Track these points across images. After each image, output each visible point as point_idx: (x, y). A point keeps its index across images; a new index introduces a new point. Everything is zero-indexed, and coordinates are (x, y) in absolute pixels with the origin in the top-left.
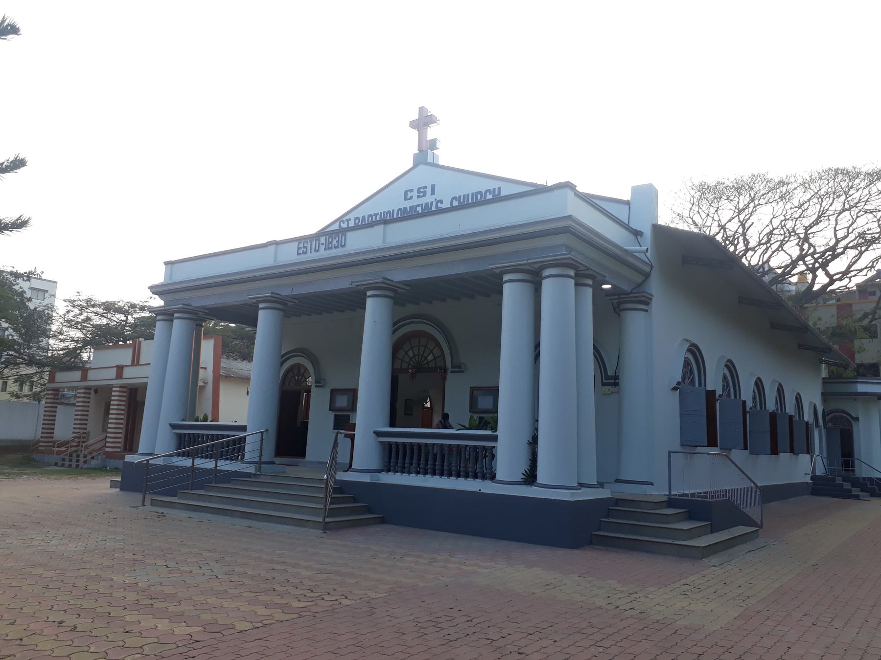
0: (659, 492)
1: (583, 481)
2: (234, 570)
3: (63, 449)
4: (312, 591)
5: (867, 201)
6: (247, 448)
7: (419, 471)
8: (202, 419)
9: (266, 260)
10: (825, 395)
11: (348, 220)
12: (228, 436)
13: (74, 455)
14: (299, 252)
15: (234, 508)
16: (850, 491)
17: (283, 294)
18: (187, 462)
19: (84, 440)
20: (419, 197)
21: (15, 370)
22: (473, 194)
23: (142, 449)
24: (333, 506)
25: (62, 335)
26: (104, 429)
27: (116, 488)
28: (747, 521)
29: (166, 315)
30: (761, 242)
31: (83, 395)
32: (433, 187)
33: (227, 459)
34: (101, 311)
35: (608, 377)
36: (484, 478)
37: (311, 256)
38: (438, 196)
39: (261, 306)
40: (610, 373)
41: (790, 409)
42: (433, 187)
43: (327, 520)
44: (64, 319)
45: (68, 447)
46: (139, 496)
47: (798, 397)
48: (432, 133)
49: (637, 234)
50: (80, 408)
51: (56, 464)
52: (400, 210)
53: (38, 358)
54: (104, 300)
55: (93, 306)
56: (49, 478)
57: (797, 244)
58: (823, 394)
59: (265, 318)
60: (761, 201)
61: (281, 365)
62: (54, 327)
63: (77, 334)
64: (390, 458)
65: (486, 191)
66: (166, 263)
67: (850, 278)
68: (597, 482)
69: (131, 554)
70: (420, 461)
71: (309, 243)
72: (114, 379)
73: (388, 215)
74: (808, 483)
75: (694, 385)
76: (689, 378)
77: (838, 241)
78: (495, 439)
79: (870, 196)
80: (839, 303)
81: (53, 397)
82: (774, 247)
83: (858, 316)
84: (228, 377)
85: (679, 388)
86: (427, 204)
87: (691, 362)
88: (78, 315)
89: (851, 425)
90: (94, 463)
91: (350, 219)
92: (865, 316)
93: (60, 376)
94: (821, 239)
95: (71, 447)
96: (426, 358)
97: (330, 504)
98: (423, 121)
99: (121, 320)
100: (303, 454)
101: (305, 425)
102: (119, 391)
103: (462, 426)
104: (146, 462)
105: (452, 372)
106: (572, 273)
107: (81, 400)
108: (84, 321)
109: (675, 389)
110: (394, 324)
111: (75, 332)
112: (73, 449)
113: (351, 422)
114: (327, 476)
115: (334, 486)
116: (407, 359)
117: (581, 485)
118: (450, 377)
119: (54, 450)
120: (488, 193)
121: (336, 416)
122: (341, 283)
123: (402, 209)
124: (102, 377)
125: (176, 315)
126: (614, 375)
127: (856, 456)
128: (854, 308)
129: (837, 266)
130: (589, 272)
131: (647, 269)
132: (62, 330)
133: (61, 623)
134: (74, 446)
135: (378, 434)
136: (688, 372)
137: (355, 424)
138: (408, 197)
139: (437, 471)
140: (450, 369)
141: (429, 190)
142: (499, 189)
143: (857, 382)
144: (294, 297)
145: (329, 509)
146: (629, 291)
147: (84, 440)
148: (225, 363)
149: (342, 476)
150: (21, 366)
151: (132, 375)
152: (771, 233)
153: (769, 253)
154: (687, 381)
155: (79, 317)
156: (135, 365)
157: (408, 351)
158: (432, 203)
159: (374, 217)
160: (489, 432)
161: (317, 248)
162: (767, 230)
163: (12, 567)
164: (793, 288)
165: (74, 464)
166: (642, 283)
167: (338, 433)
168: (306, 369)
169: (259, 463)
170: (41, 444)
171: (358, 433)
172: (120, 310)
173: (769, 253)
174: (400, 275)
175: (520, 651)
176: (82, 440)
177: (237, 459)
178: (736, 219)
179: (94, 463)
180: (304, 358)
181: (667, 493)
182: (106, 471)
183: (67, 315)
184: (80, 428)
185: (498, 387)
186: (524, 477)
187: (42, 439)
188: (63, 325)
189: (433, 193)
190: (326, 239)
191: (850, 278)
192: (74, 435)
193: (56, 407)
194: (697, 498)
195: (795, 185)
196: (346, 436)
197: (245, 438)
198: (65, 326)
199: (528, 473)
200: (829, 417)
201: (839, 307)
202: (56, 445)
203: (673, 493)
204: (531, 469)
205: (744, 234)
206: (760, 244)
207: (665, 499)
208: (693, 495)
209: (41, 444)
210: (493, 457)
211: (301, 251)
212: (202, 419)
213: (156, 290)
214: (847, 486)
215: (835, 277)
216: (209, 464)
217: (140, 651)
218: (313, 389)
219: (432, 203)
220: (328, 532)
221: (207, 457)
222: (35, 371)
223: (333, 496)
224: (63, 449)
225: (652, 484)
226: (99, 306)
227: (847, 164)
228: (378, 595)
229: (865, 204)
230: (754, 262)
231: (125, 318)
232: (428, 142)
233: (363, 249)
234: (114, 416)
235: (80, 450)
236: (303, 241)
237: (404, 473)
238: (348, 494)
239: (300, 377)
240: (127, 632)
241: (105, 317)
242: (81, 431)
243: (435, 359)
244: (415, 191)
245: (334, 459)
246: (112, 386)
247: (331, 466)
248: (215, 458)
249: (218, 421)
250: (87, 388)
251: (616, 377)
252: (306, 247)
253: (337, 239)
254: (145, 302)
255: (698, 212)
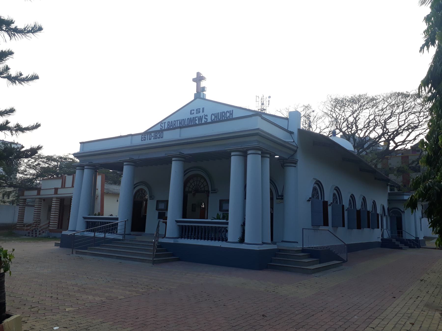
0: (299, 246)
1: (265, 241)
2: (115, 279)
3: (28, 228)
4: (148, 286)
5: (414, 107)
6: (119, 228)
7: (195, 238)
8: (97, 214)
9: (127, 143)
10: (389, 201)
11: (165, 123)
12: (110, 223)
13: (34, 231)
14: (142, 140)
15: (113, 255)
16: (398, 245)
17: (134, 158)
18: (92, 234)
19: (39, 223)
20: (197, 113)
21: (3, 189)
22: (221, 113)
23: (70, 228)
24: (157, 253)
25: (26, 172)
26: (48, 218)
27: (58, 246)
28: (338, 258)
29: (82, 167)
30: (365, 127)
31: (38, 202)
32: (203, 109)
33: (109, 233)
34: (45, 160)
35: (279, 196)
36: (223, 240)
37: (147, 142)
38: (205, 113)
39: (125, 164)
40: (280, 194)
41: (369, 208)
42: (203, 109)
43: (154, 259)
44: (27, 164)
45: (31, 227)
46: (71, 250)
47: (364, 198)
48: (203, 84)
49: (291, 133)
50: (37, 208)
51: (25, 235)
52: (188, 119)
53: (14, 183)
54: (46, 155)
55: (41, 158)
56: (25, 242)
57: (381, 128)
58: (388, 200)
59: (126, 169)
60: (364, 108)
61: (134, 189)
62: (22, 168)
63: (32, 171)
64: (182, 232)
65: (227, 112)
66: (81, 143)
67: (406, 144)
68: (262, 242)
69: (72, 273)
70: (206, 234)
71: (147, 136)
72: (53, 195)
73: (183, 121)
74: (379, 242)
75: (318, 199)
76: (316, 195)
77: (400, 127)
78: (227, 223)
79: (415, 105)
80: (402, 155)
81: (23, 203)
82: (371, 129)
83: (410, 162)
84: (108, 193)
85: (310, 200)
86: (200, 116)
87: (317, 188)
88: (34, 162)
89: (401, 215)
90: (44, 234)
91: (165, 122)
92: (413, 162)
93: (27, 193)
94: (392, 126)
95: (33, 227)
96: (200, 186)
97: (156, 253)
98: (199, 79)
99: (55, 165)
100: (144, 230)
101: (145, 217)
102: (56, 200)
103: (214, 218)
104: (73, 234)
105: (211, 193)
106: (260, 152)
107: (37, 204)
108: (37, 165)
109: (309, 201)
110: (185, 172)
111: (32, 171)
112: (33, 228)
113: (166, 216)
114: (154, 240)
115: (158, 245)
116: (191, 187)
117: (263, 243)
118: (210, 195)
119: (24, 229)
120: (228, 113)
121: (159, 213)
122: (161, 154)
123: (189, 118)
124: (47, 193)
125: (85, 167)
126: (281, 195)
127: (403, 229)
128: (410, 158)
129: (398, 139)
130: (268, 152)
131: (295, 149)
132: (26, 169)
133: (51, 297)
134: (34, 227)
135: (177, 222)
136: (315, 193)
137: (167, 217)
138: (192, 113)
139: (203, 238)
140: (211, 192)
141: (201, 110)
142: (232, 111)
143: (404, 195)
144: (140, 160)
145: (155, 254)
146: (287, 158)
147: (39, 223)
148: (107, 186)
149: (161, 240)
150: (6, 187)
151: (62, 193)
152: (369, 122)
153: (369, 131)
154: (315, 197)
155: (34, 163)
156: (63, 188)
157: (195, 181)
158: (203, 116)
159: (176, 122)
160: (225, 221)
161: (150, 138)
162: (368, 121)
163: (24, 278)
164: (381, 148)
165: (34, 235)
166: (293, 154)
167: (159, 221)
168: (145, 191)
169: (124, 235)
170: (17, 225)
171: (168, 221)
172: (55, 160)
173: (369, 131)
174: (187, 151)
175: (225, 305)
176: (37, 223)
177: (114, 233)
178: (352, 116)
179: (44, 234)
180: (144, 186)
181: (302, 247)
182: (50, 238)
183: (28, 162)
184: (36, 218)
185: (229, 200)
186: (239, 240)
187: (18, 223)
188: (26, 168)
189: (203, 112)
190: (154, 134)
191: (406, 144)
192: (34, 221)
193: (25, 208)
194: (314, 248)
195: (381, 99)
196: (163, 222)
197: (117, 223)
198: (27, 168)
199: (241, 238)
200: (391, 211)
201: (402, 157)
202: (25, 226)
203: (304, 247)
204: (242, 236)
205: (356, 123)
206: (364, 127)
207: (301, 249)
208: (312, 248)
209: (17, 225)
210: (227, 231)
211: (143, 139)
212: (97, 214)
213: (77, 155)
214: (397, 243)
215: (398, 144)
216: (102, 235)
217: (84, 305)
218: (148, 199)
219: (203, 116)
220: (155, 264)
221: (100, 232)
222: (13, 190)
223: (157, 249)
224: (28, 228)
225: (297, 243)
226: (44, 158)
227: (404, 90)
228: (174, 287)
229: (413, 109)
230: (362, 135)
231: (57, 164)
232: (201, 88)
233: (171, 139)
234: (54, 212)
235: (37, 228)
236: (144, 135)
237: (189, 238)
238: (176, 257)
239: (142, 195)
240: (78, 299)
241: (47, 163)
242: (37, 219)
243: (204, 187)
244: (195, 110)
245: (157, 232)
246: (52, 198)
247: (156, 236)
248: (104, 232)
249: (103, 216)
250: (40, 199)
251: (282, 196)
252: (145, 138)
253: (159, 134)
254: (67, 156)
255: (335, 112)
